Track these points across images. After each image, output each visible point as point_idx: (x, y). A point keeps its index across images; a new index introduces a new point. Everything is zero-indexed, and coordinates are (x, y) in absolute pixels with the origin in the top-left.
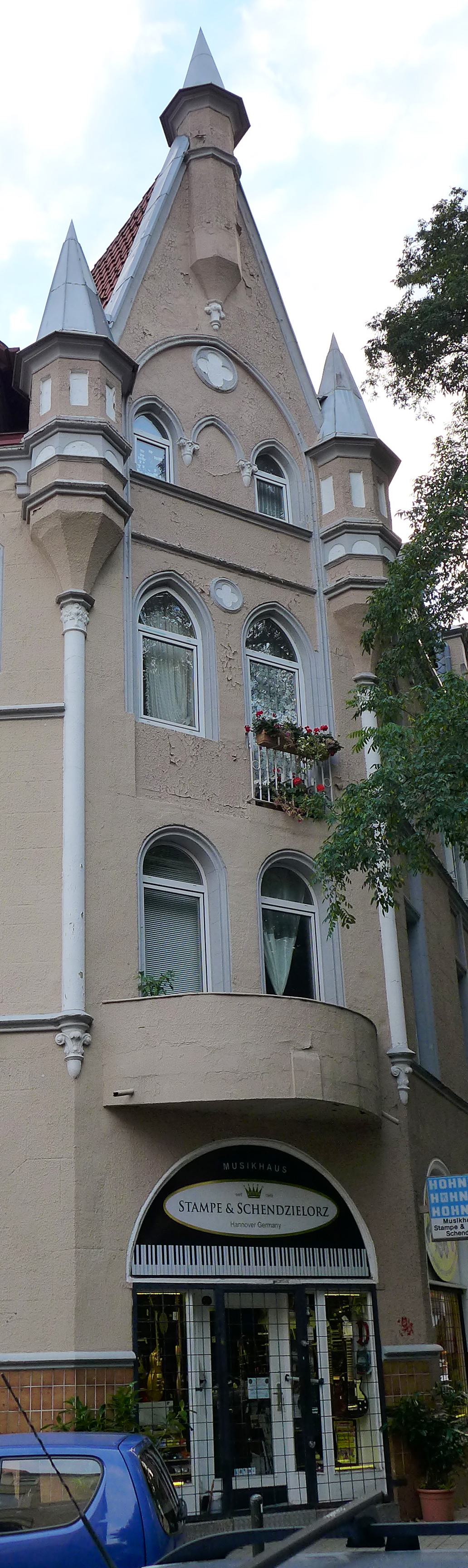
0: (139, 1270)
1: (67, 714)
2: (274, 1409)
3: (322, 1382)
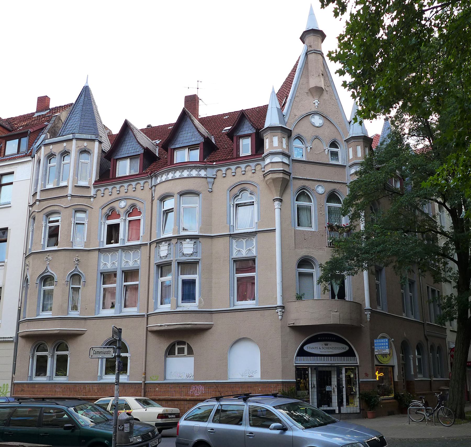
0: (297, 362)
1: (276, 231)
2: (333, 393)
3: (343, 387)
